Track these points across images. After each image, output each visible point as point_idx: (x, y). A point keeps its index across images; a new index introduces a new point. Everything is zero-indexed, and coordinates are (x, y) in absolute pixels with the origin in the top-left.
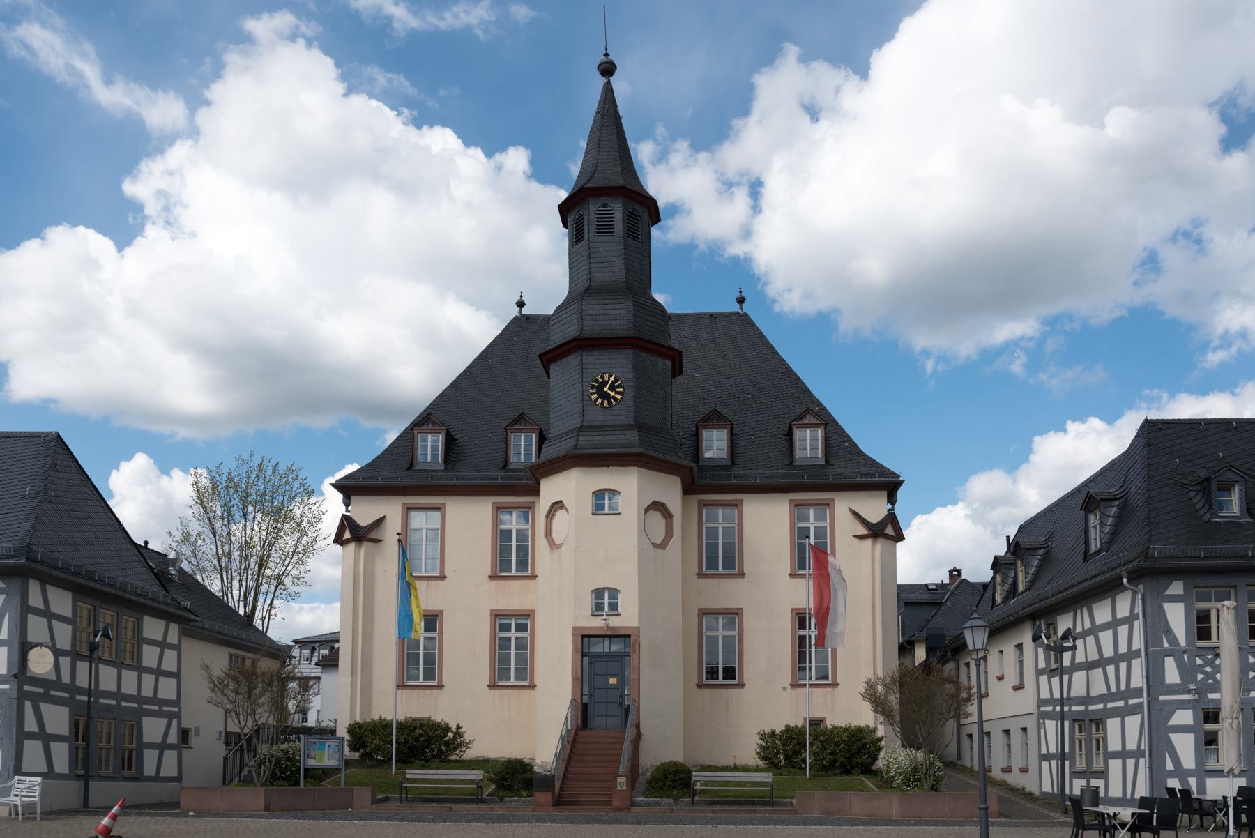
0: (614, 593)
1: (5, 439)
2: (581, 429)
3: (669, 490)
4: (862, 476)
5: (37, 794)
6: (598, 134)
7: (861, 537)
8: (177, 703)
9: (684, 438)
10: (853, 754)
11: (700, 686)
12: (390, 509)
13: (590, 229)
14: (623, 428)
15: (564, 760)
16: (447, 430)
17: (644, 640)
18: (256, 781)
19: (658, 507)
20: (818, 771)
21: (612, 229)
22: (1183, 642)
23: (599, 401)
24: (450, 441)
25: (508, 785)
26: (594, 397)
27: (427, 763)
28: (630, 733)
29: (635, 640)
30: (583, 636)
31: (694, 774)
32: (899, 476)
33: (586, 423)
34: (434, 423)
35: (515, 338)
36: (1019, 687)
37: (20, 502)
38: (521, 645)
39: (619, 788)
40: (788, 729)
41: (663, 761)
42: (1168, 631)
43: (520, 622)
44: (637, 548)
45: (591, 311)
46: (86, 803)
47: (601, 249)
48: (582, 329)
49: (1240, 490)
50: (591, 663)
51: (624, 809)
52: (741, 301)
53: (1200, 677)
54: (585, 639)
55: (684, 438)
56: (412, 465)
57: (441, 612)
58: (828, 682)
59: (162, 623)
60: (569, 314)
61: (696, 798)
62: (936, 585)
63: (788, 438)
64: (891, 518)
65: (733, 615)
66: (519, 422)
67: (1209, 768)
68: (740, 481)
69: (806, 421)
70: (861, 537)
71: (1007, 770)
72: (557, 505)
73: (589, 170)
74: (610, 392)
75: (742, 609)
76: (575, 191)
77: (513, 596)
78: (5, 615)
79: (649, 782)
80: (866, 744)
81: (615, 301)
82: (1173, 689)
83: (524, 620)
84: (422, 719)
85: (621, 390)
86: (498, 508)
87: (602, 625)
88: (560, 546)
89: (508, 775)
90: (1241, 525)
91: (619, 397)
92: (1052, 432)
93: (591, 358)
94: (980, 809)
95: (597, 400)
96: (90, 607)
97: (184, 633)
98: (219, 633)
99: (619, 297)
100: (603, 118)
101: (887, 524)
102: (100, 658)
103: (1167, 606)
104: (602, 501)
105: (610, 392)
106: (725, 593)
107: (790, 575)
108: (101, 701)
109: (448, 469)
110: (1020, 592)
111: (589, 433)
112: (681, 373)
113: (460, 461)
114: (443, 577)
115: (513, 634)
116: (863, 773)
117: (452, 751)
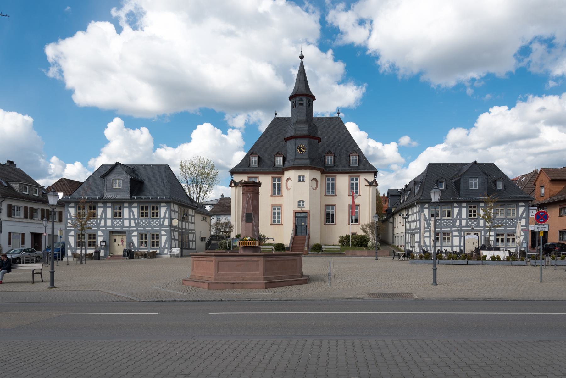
0: (303, 202)
2: (295, 159)
3: (317, 175)
7: (367, 186)
8: (194, 230)
11: (325, 224)
17: (311, 213)
19: (315, 179)
22: (428, 218)
23: (300, 152)
24: (259, 158)
26: (298, 151)
28: (307, 237)
30: (296, 213)
32: (377, 170)
34: (255, 154)
36: (403, 226)
38: (279, 213)
40: (347, 236)
43: (279, 208)
46: (182, 255)
47: (300, 110)
48: (295, 133)
50: (297, 219)
56: (249, 165)
61: (323, 252)
62: (401, 189)
64: (375, 181)
65: (334, 206)
66: (278, 154)
69: (354, 154)
70: (367, 186)
71: (401, 246)
72: (289, 179)
75: (336, 204)
76: (292, 95)
77: (277, 201)
79: (312, 248)
86: (272, 177)
88: (290, 189)
90: (444, 191)
91: (305, 151)
92: (453, 129)
93: (298, 141)
95: (299, 152)
97: (196, 212)
104: (301, 179)
106: (331, 200)
107: (348, 195)
108: (107, 228)
112: (321, 142)
115: (277, 211)
116: (364, 246)
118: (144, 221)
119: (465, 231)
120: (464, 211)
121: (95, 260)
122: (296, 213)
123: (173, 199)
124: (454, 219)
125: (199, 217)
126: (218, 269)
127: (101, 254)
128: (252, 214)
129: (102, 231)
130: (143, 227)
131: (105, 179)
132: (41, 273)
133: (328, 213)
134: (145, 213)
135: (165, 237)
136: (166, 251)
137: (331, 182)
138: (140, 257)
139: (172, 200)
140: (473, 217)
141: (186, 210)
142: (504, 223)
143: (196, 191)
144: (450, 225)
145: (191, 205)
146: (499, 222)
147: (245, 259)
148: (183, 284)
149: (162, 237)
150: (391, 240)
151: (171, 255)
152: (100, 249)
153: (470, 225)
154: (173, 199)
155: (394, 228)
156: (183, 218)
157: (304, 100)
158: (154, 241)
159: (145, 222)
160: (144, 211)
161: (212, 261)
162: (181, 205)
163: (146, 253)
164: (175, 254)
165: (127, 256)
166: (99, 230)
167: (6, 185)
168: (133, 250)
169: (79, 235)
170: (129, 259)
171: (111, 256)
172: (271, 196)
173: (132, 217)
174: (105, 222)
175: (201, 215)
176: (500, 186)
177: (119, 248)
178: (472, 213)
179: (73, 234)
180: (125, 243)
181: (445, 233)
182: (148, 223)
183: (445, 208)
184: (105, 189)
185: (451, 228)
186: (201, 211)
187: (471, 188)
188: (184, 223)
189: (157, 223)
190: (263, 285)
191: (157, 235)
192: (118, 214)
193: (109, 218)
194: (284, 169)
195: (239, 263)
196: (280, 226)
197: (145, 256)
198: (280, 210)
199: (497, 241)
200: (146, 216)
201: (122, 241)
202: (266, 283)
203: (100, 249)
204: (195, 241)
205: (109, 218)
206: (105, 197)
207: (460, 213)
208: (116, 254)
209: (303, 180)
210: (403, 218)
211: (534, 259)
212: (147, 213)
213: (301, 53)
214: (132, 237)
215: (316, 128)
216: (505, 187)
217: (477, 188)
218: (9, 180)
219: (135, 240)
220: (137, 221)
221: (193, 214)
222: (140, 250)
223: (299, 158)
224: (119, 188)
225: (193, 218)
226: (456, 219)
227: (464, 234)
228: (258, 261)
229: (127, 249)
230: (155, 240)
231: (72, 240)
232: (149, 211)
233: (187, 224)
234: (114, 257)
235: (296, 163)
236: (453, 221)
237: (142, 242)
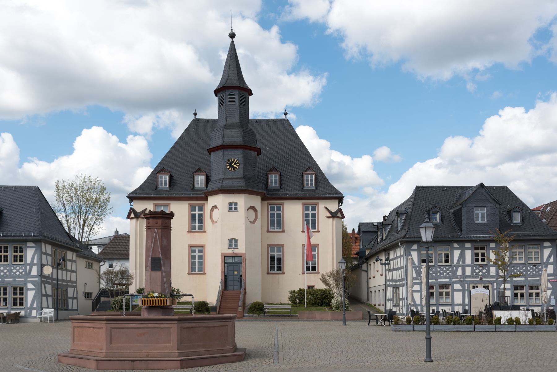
0: (236, 241)
1: (19, 189)
2: (224, 179)
3: (256, 201)
4: (329, 194)
5: (53, 314)
6: (229, 63)
7: (328, 217)
8: (75, 282)
9: (262, 177)
10: (323, 299)
11: (268, 273)
13: (226, 101)
14: (239, 179)
15: (219, 302)
16: (170, 174)
17: (247, 258)
18: (115, 310)
19: (252, 208)
20: (310, 305)
21: (234, 102)
22: (417, 264)
23: (230, 168)
24: (171, 177)
25: (201, 310)
26: (228, 167)
28: (242, 292)
29: (244, 258)
30: (225, 256)
31: (265, 306)
32: (342, 194)
33: (225, 177)
34: (165, 171)
35: (194, 130)
36: (382, 275)
37: (33, 214)
38: (200, 257)
39: (239, 311)
40: (300, 290)
41: (254, 302)
44: (244, 224)
45: (227, 135)
47: (231, 110)
49: (439, 214)
50: (228, 266)
51: (241, 318)
52: (286, 114)
54: (225, 257)
55: (262, 177)
58: (316, 272)
59: (72, 253)
60: (218, 134)
61: (266, 314)
62: (377, 223)
63: (302, 177)
64: (340, 210)
65: (280, 247)
66: (199, 171)
68: (283, 196)
69: (309, 172)
70: (328, 217)
71: (379, 305)
72: (215, 207)
73: (225, 77)
74: (234, 166)
75: (284, 244)
77: (197, 239)
78: (35, 255)
79: (249, 309)
80: (328, 295)
81: (236, 131)
83: (201, 248)
85: (238, 164)
86: (190, 205)
87: (232, 252)
88: (216, 222)
89: (200, 307)
90: (439, 226)
91: (237, 167)
94: (343, 314)
95: (229, 168)
96: (60, 251)
97: (77, 256)
98: (83, 254)
99: (237, 129)
100: (231, 56)
101: (338, 212)
102: (63, 269)
103: (412, 252)
104: (232, 207)
105: (234, 166)
106: (277, 238)
107: (302, 231)
109: (171, 189)
110: (384, 240)
111: (227, 181)
112: (261, 154)
113: (175, 186)
115: (197, 254)
116: (326, 306)
119: (470, 283)
120: (468, 254)
122: (226, 258)
123: (44, 236)
124: (455, 266)
125: (82, 263)
126: (111, 340)
133: (273, 258)
136: (34, 313)
137: (276, 212)
139: (43, 238)
142: (524, 271)
143: (78, 224)
144: (448, 274)
145: (70, 245)
146: (516, 269)
148: (59, 361)
149: (29, 292)
153: (477, 274)
154: (44, 236)
156: (59, 264)
158: (17, 298)
161: (102, 328)
162: (55, 244)
163: (5, 315)
164: (48, 316)
174: (464, 271)
176: (517, 218)
178: (480, 257)
181: (441, 287)
182: (8, 271)
183: (442, 250)
185: (451, 278)
186: (85, 253)
187: (476, 222)
188: (60, 272)
189: (21, 271)
190: (178, 364)
191: (22, 289)
195: (141, 331)
199: (515, 297)
200: (6, 261)
202: (182, 360)
204: (76, 298)
207: (462, 257)
209: (236, 208)
210: (381, 264)
214: (400, 258)
216: (523, 220)
217: (486, 221)
221: (74, 259)
223: (230, 177)
225: (74, 264)
226: (458, 266)
227: (469, 287)
228: (170, 328)
230: (18, 296)
233: (64, 273)
235: (225, 184)
236: (453, 269)
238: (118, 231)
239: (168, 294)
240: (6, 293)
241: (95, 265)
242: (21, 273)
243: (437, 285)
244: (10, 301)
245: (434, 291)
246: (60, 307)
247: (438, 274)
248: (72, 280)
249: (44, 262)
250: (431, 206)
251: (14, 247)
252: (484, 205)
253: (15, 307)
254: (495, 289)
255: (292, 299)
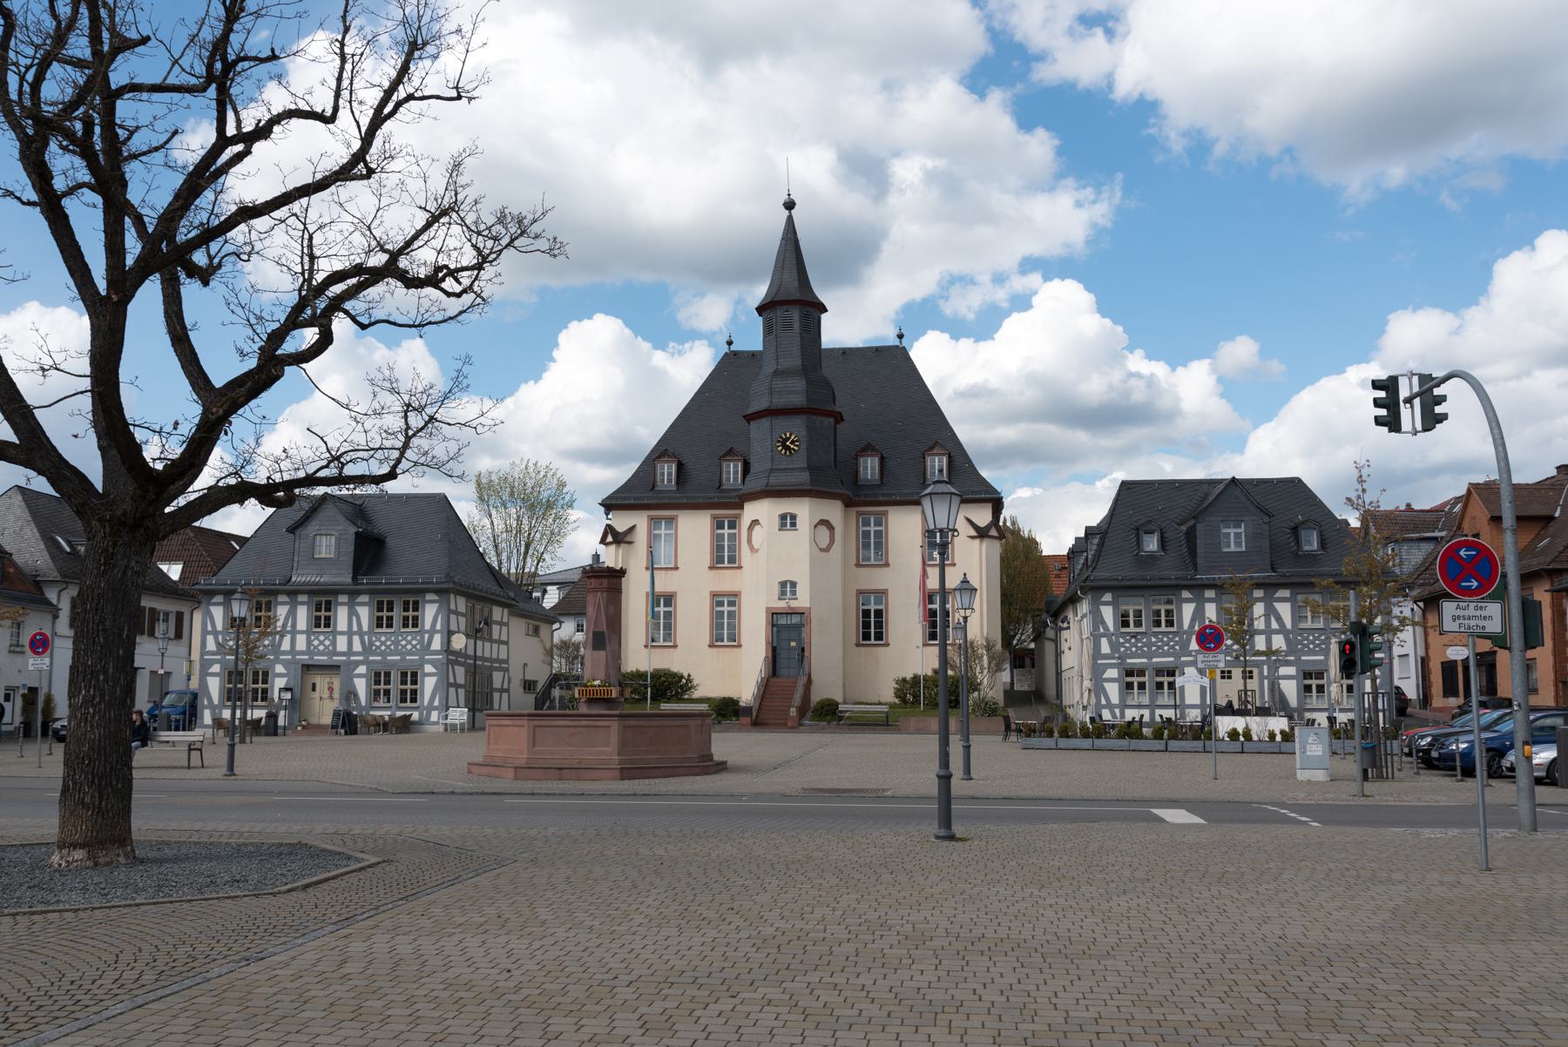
0: (794, 585)
3: (833, 511)
7: (972, 537)
8: (506, 661)
11: (858, 645)
12: (639, 521)
19: (824, 523)
22: (1112, 629)
24: (680, 466)
26: (780, 448)
27: (669, 700)
42: (1103, 622)
50: (778, 632)
52: (901, 336)
53: (1122, 649)
54: (774, 615)
56: (654, 487)
57: (676, 593)
59: (501, 609)
65: (881, 594)
66: (730, 453)
67: (1158, 703)
69: (935, 451)
70: (972, 537)
72: (755, 522)
77: (726, 581)
82: (1106, 657)
83: (734, 598)
84: (665, 670)
86: (714, 517)
88: (757, 551)
90: (1156, 557)
97: (510, 614)
104: (788, 521)
114: (676, 568)
115: (726, 608)
117: (684, 692)
118: (383, 639)
121: (267, 735)
123: (454, 583)
124: (1185, 632)
125: (518, 627)
126: (534, 741)
127: (281, 722)
128: (606, 634)
129: (284, 663)
130: (382, 654)
131: (297, 537)
132: (201, 750)
133: (866, 613)
134: (388, 617)
135: (434, 679)
136: (434, 716)
137: (872, 528)
138: (372, 729)
139: (452, 585)
140: (1163, 628)
141: (486, 609)
143: (515, 551)
144: (1173, 647)
145: (498, 595)
146: (1307, 639)
147: (584, 723)
148: (469, 772)
149: (427, 679)
150: (1051, 691)
151: (446, 724)
152: (279, 707)
154: (454, 583)
155: (1058, 654)
156: (478, 631)
157: (795, 315)
158: (406, 690)
159: (387, 640)
160: (385, 614)
161: (523, 726)
162: (474, 596)
163: (387, 718)
164: (457, 722)
165: (342, 728)
166: (277, 661)
167: (68, 549)
168: (355, 713)
169: (230, 674)
170: (346, 734)
171: (304, 727)
172: (711, 568)
173: (355, 628)
175: (525, 620)
176: (1311, 543)
177: (324, 709)
178: (1163, 619)
179: (218, 671)
180: (336, 695)
181: (1159, 672)
182: (393, 643)
184: (296, 559)
185: (1177, 656)
186: (526, 609)
187: (1226, 550)
188: (479, 643)
189: (414, 642)
190: (617, 773)
191: (414, 675)
192: (323, 621)
193: (302, 632)
194: (743, 495)
195: (572, 730)
196: (735, 649)
197: (384, 726)
198: (735, 605)
199: (1305, 692)
200: (390, 625)
201: (331, 689)
202: (622, 769)
203: (279, 707)
204: (507, 691)
205: (302, 632)
206: (293, 579)
208: (314, 721)
209: (793, 524)
211: (1339, 738)
212: (392, 617)
213: (789, 195)
214: (355, 680)
215: (826, 385)
216: (1323, 544)
217: (1244, 549)
218: (74, 536)
219: (361, 686)
220: (366, 637)
221: (505, 620)
222: (371, 713)
223: (782, 467)
224: (328, 556)
225: (504, 629)
228: (609, 727)
229: (341, 708)
230: (409, 686)
231: (214, 686)
232: (397, 614)
233: (487, 645)
234: (313, 729)
235: (772, 480)
237: (377, 693)
238: (598, 556)
239: (613, 680)
240: (390, 681)
241: (544, 629)
242: (414, 646)
243: (1151, 669)
244: (394, 695)
245: (1146, 679)
246: (478, 706)
247: (1154, 648)
248: (500, 657)
249: (453, 627)
250: (1144, 520)
251: (404, 602)
252: (1240, 518)
253: (403, 705)
254: (1266, 678)
255: (900, 694)
